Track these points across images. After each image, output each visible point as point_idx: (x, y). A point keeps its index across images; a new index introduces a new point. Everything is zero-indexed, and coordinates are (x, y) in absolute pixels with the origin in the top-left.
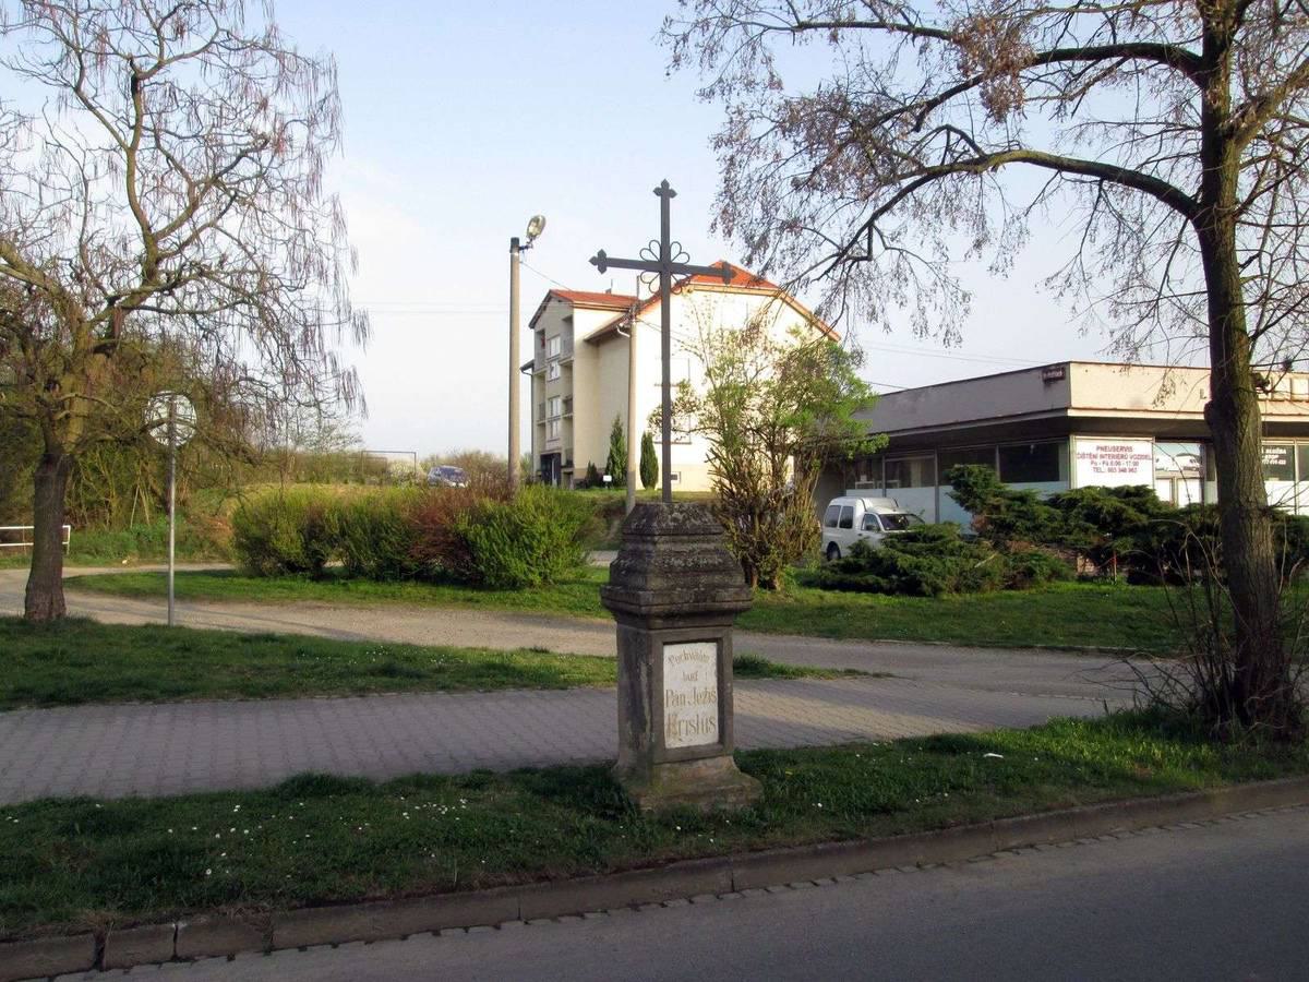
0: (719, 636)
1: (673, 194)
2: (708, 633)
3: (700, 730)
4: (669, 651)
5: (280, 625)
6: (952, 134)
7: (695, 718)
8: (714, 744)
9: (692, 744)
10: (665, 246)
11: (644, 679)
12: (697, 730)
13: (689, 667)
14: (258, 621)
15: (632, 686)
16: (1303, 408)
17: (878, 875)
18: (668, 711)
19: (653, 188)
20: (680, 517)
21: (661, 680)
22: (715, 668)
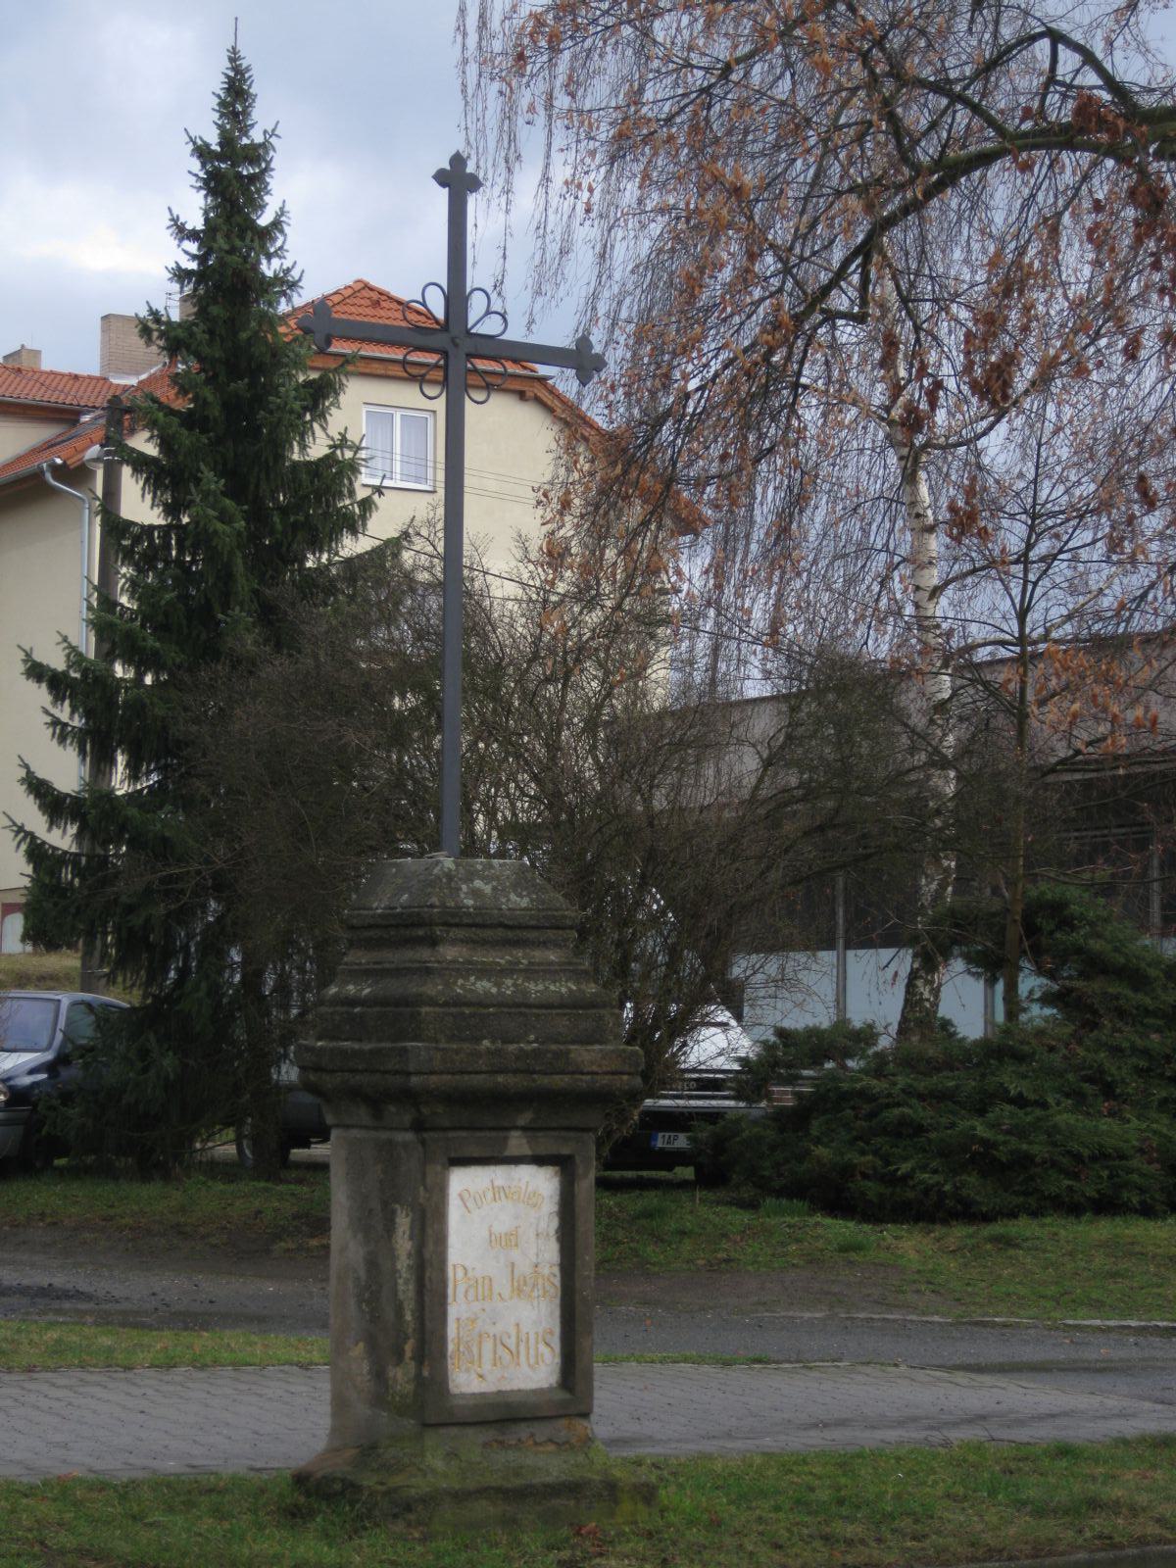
0: (565, 1151)
1: (474, 184)
2: (548, 1145)
3: (523, 1358)
4: (463, 1182)
5: (447, 1078)
6: (1063, 52)
7: (513, 1331)
8: (550, 1389)
9: (506, 1386)
10: (457, 294)
11: (403, 1244)
12: (515, 1355)
13: (502, 1216)
14: (566, 1078)
15: (372, 1264)
16: (9, 1276)
17: (277, 224)
18: (454, 1311)
19: (433, 171)
20: (487, 889)
21: (441, 1240)
22: (555, 1223)
